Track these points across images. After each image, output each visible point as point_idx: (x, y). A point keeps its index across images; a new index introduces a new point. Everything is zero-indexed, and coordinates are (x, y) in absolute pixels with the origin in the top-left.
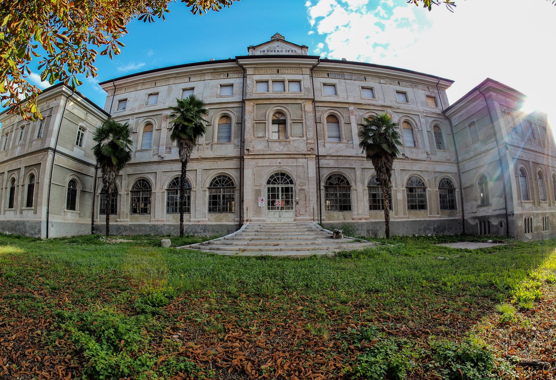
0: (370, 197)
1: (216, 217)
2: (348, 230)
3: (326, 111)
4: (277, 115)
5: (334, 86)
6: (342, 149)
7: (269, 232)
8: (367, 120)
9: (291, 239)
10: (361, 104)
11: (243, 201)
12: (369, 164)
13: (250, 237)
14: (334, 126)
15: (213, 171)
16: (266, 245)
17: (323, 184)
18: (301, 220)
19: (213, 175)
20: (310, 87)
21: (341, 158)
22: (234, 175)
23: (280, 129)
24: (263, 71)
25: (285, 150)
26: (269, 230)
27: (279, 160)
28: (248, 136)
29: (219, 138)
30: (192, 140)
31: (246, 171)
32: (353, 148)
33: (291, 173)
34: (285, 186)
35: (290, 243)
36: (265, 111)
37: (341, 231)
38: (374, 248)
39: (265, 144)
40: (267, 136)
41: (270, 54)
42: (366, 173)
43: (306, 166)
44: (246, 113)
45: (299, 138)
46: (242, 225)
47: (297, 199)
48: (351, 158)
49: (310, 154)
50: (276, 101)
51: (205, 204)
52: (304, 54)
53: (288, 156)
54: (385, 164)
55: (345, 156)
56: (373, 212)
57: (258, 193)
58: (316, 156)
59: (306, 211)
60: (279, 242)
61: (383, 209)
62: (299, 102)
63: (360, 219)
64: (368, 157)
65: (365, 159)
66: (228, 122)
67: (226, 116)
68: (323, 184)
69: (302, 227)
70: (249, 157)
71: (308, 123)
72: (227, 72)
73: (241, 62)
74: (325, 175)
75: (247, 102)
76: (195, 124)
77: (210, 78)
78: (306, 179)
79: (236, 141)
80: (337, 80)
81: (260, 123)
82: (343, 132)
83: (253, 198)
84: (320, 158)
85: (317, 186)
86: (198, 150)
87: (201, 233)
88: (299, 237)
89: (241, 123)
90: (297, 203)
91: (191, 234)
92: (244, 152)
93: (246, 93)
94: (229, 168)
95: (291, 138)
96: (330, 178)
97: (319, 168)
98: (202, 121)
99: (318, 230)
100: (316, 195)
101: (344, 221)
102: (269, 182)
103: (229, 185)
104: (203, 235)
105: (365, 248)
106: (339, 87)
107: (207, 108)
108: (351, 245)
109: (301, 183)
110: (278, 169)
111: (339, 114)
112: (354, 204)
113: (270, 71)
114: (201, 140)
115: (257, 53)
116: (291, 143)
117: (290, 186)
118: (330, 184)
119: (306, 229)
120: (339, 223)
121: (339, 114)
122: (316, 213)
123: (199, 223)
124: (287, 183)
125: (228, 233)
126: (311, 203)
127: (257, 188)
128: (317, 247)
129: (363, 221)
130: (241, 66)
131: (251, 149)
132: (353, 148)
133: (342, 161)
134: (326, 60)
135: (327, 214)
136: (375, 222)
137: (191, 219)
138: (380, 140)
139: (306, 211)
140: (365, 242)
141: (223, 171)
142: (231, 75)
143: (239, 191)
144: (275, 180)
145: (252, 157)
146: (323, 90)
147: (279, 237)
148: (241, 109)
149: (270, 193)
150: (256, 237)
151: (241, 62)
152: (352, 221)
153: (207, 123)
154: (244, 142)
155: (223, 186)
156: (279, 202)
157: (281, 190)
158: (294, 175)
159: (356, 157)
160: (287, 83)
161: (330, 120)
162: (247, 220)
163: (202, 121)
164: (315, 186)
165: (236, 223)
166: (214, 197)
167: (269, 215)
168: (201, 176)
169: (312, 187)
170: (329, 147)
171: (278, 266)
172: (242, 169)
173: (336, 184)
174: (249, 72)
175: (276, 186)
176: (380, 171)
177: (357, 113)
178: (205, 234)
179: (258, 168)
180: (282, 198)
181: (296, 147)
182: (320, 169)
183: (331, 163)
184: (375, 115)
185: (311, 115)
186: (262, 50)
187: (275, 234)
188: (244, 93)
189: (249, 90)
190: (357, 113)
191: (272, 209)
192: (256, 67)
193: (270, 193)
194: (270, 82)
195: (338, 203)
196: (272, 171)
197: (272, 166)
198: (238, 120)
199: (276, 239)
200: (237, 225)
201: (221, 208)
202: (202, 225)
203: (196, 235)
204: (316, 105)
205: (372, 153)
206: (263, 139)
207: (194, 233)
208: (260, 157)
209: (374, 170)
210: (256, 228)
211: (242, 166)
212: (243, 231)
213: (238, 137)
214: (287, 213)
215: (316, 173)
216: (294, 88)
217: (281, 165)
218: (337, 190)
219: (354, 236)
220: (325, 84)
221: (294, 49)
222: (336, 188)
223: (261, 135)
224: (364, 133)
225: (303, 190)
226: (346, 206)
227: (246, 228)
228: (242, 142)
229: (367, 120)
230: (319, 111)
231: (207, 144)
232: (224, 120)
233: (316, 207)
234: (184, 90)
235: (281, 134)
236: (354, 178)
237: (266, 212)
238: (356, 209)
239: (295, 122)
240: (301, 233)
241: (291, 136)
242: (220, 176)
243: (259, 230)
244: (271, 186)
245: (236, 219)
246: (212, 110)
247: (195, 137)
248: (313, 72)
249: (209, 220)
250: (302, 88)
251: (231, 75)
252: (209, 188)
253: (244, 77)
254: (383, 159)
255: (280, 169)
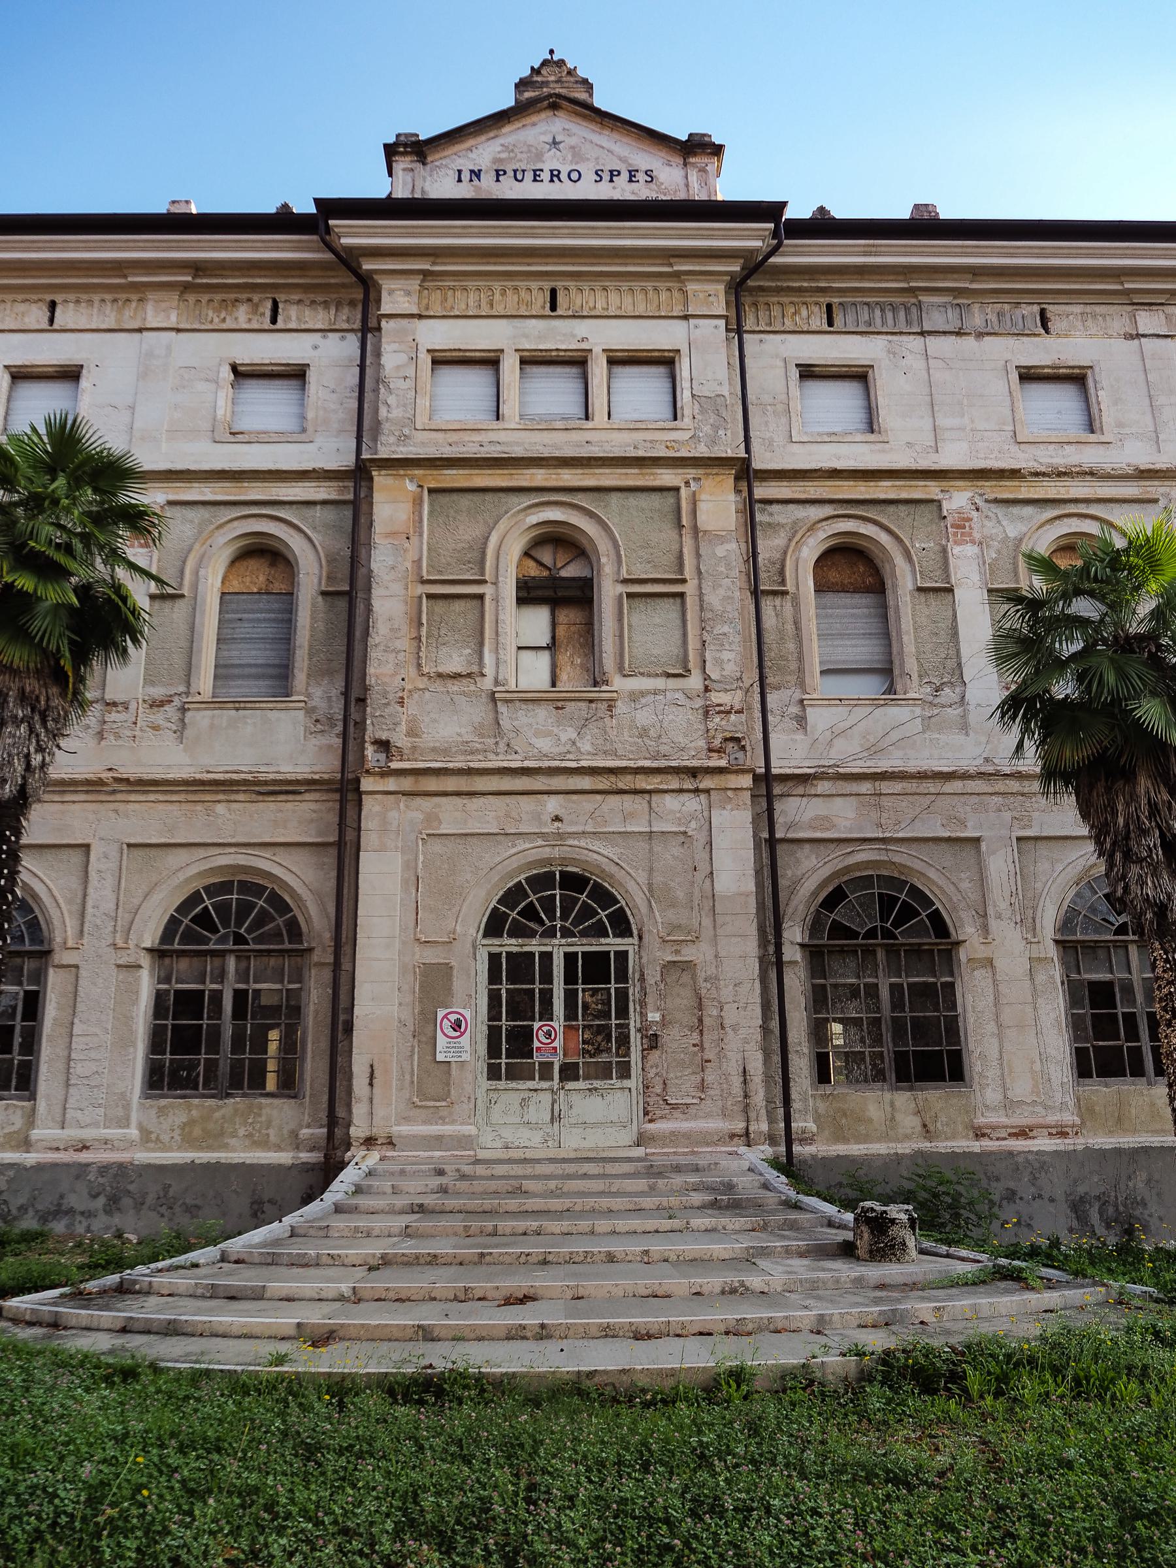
0: (1074, 1000)
1: (191, 1122)
2: (944, 1204)
3: (812, 528)
4: (546, 556)
5: (860, 376)
6: (903, 735)
7: (483, 1212)
8: (1044, 566)
9: (611, 1258)
10: (1014, 474)
11: (349, 1028)
12: (1063, 815)
13: (373, 1250)
14: (853, 609)
15: (183, 856)
16: (463, 1297)
17: (794, 934)
18: (674, 1137)
19: (181, 876)
20: (728, 389)
21: (898, 787)
22: (302, 879)
23: (561, 631)
24: (464, 301)
25: (586, 746)
26: (488, 1204)
27: (553, 805)
28: (388, 669)
29: (223, 672)
30: (59, 677)
31: (367, 861)
32: (965, 727)
33: (620, 875)
34: (581, 946)
35: (597, 1285)
36: (477, 531)
37: (898, 1212)
38: (1109, 1328)
39: (478, 712)
40: (489, 670)
41: (510, 190)
42: (1043, 866)
43: (702, 838)
44: (378, 538)
45: (660, 683)
46: (342, 1166)
47: (654, 1016)
48: (956, 786)
49: (720, 771)
50: (539, 477)
51: (124, 1042)
52: (698, 194)
53: (602, 783)
54: (1154, 810)
55: (922, 776)
56: (1102, 1091)
57: (433, 984)
58: (756, 778)
59: (702, 1087)
60: (539, 1281)
61: (1160, 1072)
62: (667, 477)
63: (1023, 1133)
64: (1052, 774)
65: (1036, 786)
66: (278, 587)
67: (262, 552)
68: (794, 934)
69: (678, 1180)
70: (391, 784)
71: (714, 599)
72: (270, 293)
73: (352, 234)
74: (810, 885)
75: (380, 479)
76: (84, 591)
77: (173, 320)
78: (701, 893)
79: (317, 692)
80: (880, 342)
81: (452, 596)
82: (910, 648)
83: (406, 1015)
84: (777, 790)
85: (763, 943)
86: (100, 735)
87: (88, 1214)
88: (658, 1248)
89: (350, 594)
90: (653, 1042)
91: (29, 1223)
92: (362, 758)
93: (377, 425)
94: (277, 843)
95: (618, 683)
96: (834, 899)
97: (771, 847)
98: (121, 573)
99: (771, 1198)
100: (756, 998)
101: (926, 1145)
102: (494, 926)
103: (277, 936)
104: (102, 1226)
105: (1053, 1329)
106: (886, 384)
107: (152, 497)
108: (963, 1302)
109: (675, 928)
110: (547, 852)
111: (883, 538)
112: (981, 1044)
113: (512, 298)
114: (123, 678)
115: (441, 183)
116: (621, 707)
117: (612, 944)
118: (838, 930)
119: (697, 1198)
120: (898, 1158)
121: (883, 538)
122: (759, 1098)
123: (84, 1157)
124: (599, 931)
125: (259, 1215)
126: (733, 1042)
127: (432, 956)
128: (753, 1313)
129: (1043, 1144)
130: (348, 260)
131: (399, 739)
132: (965, 727)
133: (904, 803)
134: (822, 226)
135: (822, 1106)
136: (1118, 1152)
137: (36, 1134)
138: (1122, 675)
139: (702, 1087)
140: (1050, 1285)
141: (242, 860)
142: (291, 315)
143: (327, 974)
144: (530, 913)
145: (407, 784)
146: (796, 405)
147: (537, 1251)
148: (348, 513)
149: (504, 988)
150: (408, 1248)
151: (352, 234)
152: (976, 1146)
153: (153, 587)
154: (362, 701)
155: (239, 939)
156: (552, 1037)
157: (561, 972)
158: (631, 886)
159: (981, 775)
160: (598, 369)
161: (833, 576)
162: (369, 1142)
163: (121, 573)
164: (751, 947)
165: (305, 1156)
166: (189, 1003)
167: (496, 1110)
168: (110, 882)
169: (733, 958)
170: (830, 726)
171: (511, 1449)
172: (349, 851)
173: (871, 934)
174: (396, 297)
175: (534, 946)
176: (1128, 856)
177: (990, 528)
178: (117, 1220)
179: (437, 847)
180: (571, 1013)
181: (644, 733)
182: (781, 849)
183: (842, 815)
184: (1092, 528)
185: (732, 550)
186: (466, 165)
187: (522, 1225)
188: (364, 424)
189: (392, 408)
190: (990, 528)
191: (511, 1077)
192: (434, 270)
193: (504, 988)
194: (510, 366)
195: (887, 1036)
196: (514, 863)
197: (510, 839)
198: (330, 578)
199: (523, 1261)
200: (307, 1168)
201: (224, 1068)
202: (104, 1169)
203: (59, 1227)
204: (760, 492)
205: (1073, 755)
206: (472, 684)
207: (44, 1218)
208: (451, 784)
209: (1090, 847)
210: (417, 1188)
211: (350, 835)
212: (338, 1209)
213: (330, 673)
214: (595, 1101)
215: (758, 873)
216: (640, 395)
217: (565, 828)
218: (876, 960)
219: (980, 1244)
220: (808, 373)
221: (645, 158)
222: (869, 952)
223: (455, 662)
224: (1030, 634)
225: (687, 966)
226: (930, 1055)
227: (358, 1190)
228: (355, 697)
229: (1044, 566)
230: (773, 527)
231: (157, 704)
232: (257, 575)
233: (756, 1064)
234: (20, 375)
235: (563, 658)
236: (974, 896)
237: (481, 1094)
238: (992, 1073)
239: (640, 594)
240: (666, 1224)
241: (621, 668)
242: (225, 887)
243: (429, 1201)
244: (510, 945)
245: (305, 1132)
246: (190, 513)
247: (81, 657)
248: (747, 300)
249: (146, 1134)
250: (685, 397)
251: (293, 311)
252: (158, 953)
253: (368, 329)
254: (1144, 784)
255: (556, 853)
